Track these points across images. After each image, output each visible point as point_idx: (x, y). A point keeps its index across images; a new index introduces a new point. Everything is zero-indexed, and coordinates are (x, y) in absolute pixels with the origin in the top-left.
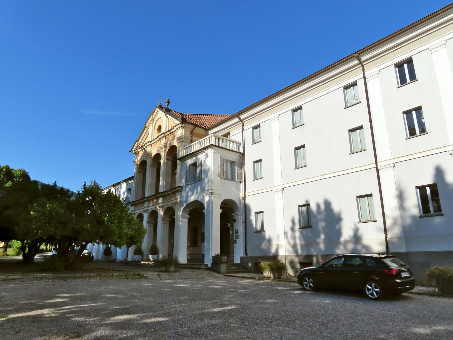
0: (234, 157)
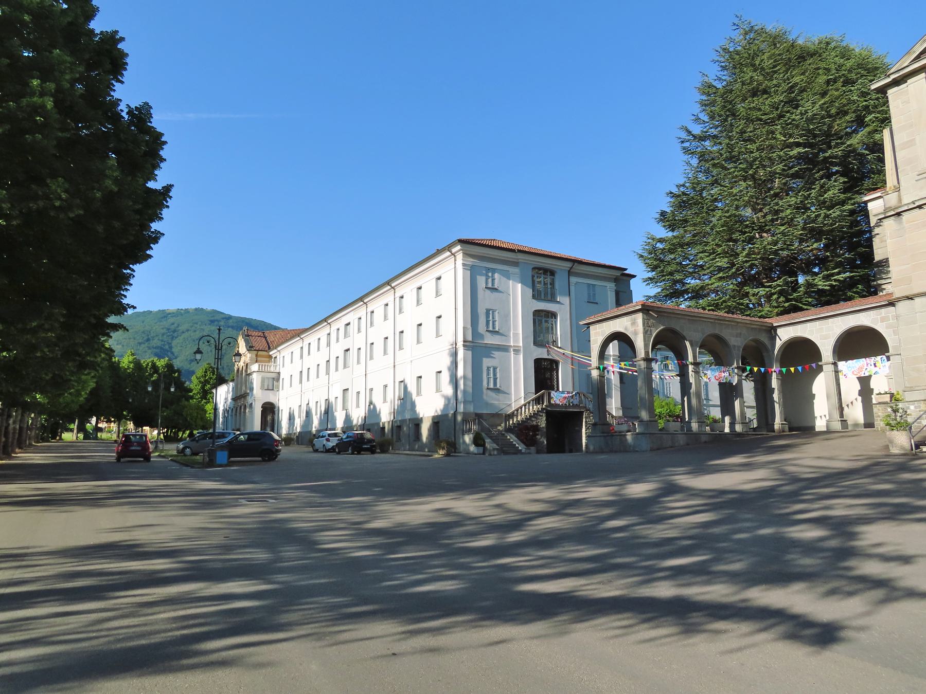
0: (274, 375)
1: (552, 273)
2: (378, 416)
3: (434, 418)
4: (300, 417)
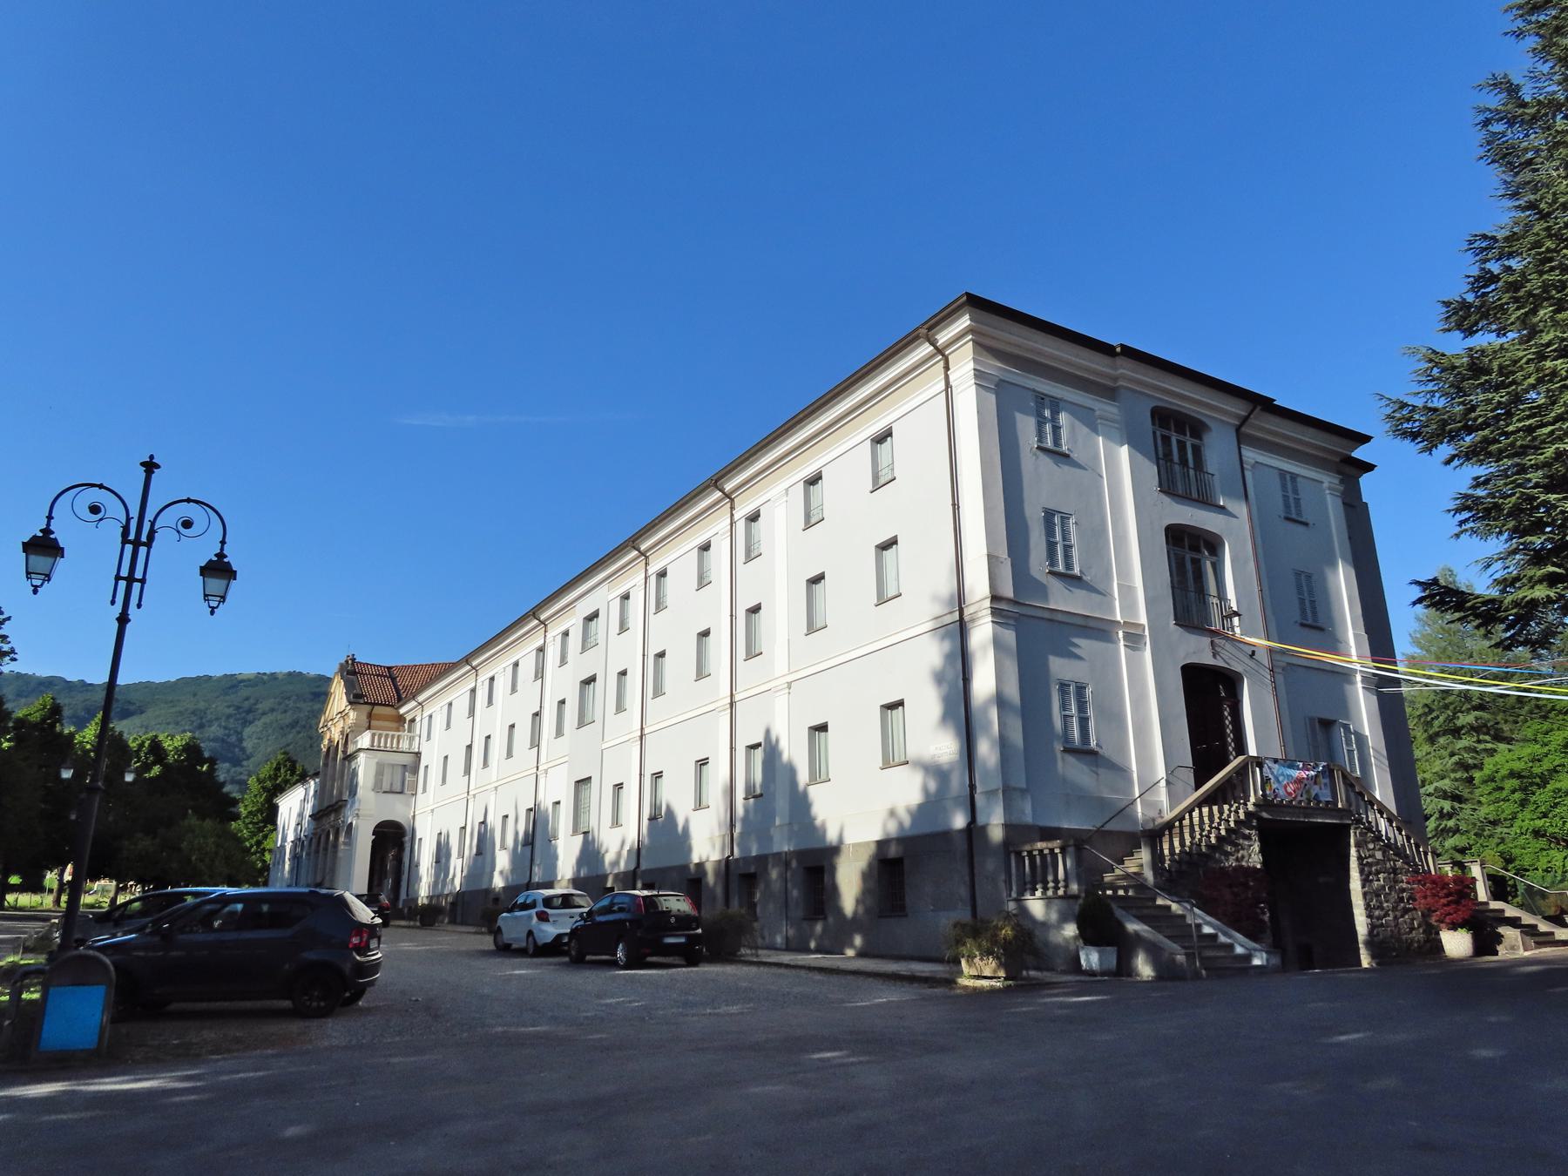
0: (406, 759)
1: (1196, 428)
2: (682, 840)
3: (881, 844)
4: (461, 855)
